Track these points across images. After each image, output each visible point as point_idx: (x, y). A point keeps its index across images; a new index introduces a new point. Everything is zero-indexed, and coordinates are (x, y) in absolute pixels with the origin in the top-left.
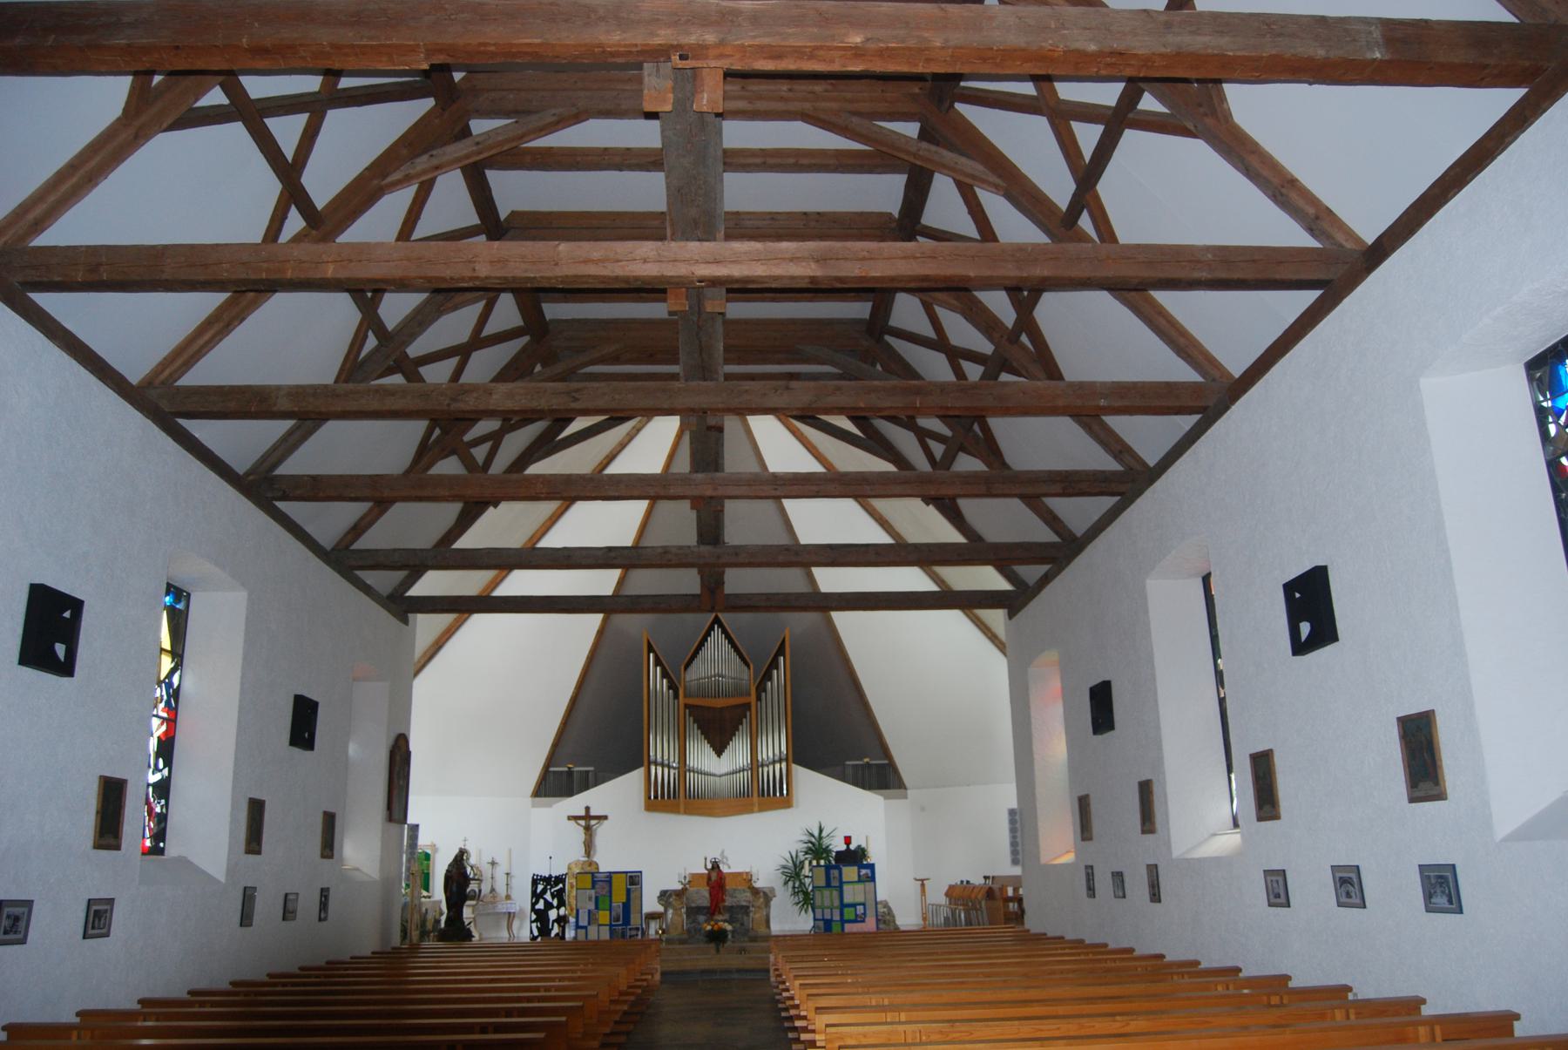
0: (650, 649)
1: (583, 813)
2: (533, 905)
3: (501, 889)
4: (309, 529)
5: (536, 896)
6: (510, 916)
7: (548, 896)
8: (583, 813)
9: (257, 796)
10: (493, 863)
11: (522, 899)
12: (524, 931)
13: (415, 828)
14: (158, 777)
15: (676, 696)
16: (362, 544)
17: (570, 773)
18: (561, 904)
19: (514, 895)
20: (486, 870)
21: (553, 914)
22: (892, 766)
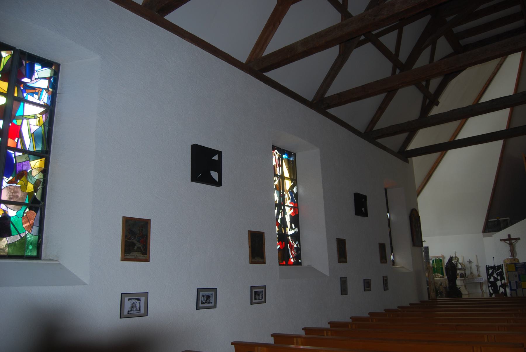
1: (507, 238)
2: (489, 279)
3: (475, 271)
4: (351, 124)
5: (489, 275)
6: (481, 284)
7: (495, 275)
8: (507, 238)
9: (382, 242)
10: (470, 262)
11: (484, 277)
12: (487, 290)
13: (427, 248)
14: (292, 232)
16: (377, 127)
17: (498, 221)
18: (502, 278)
19: (481, 275)
20: (467, 265)
21: (499, 283)
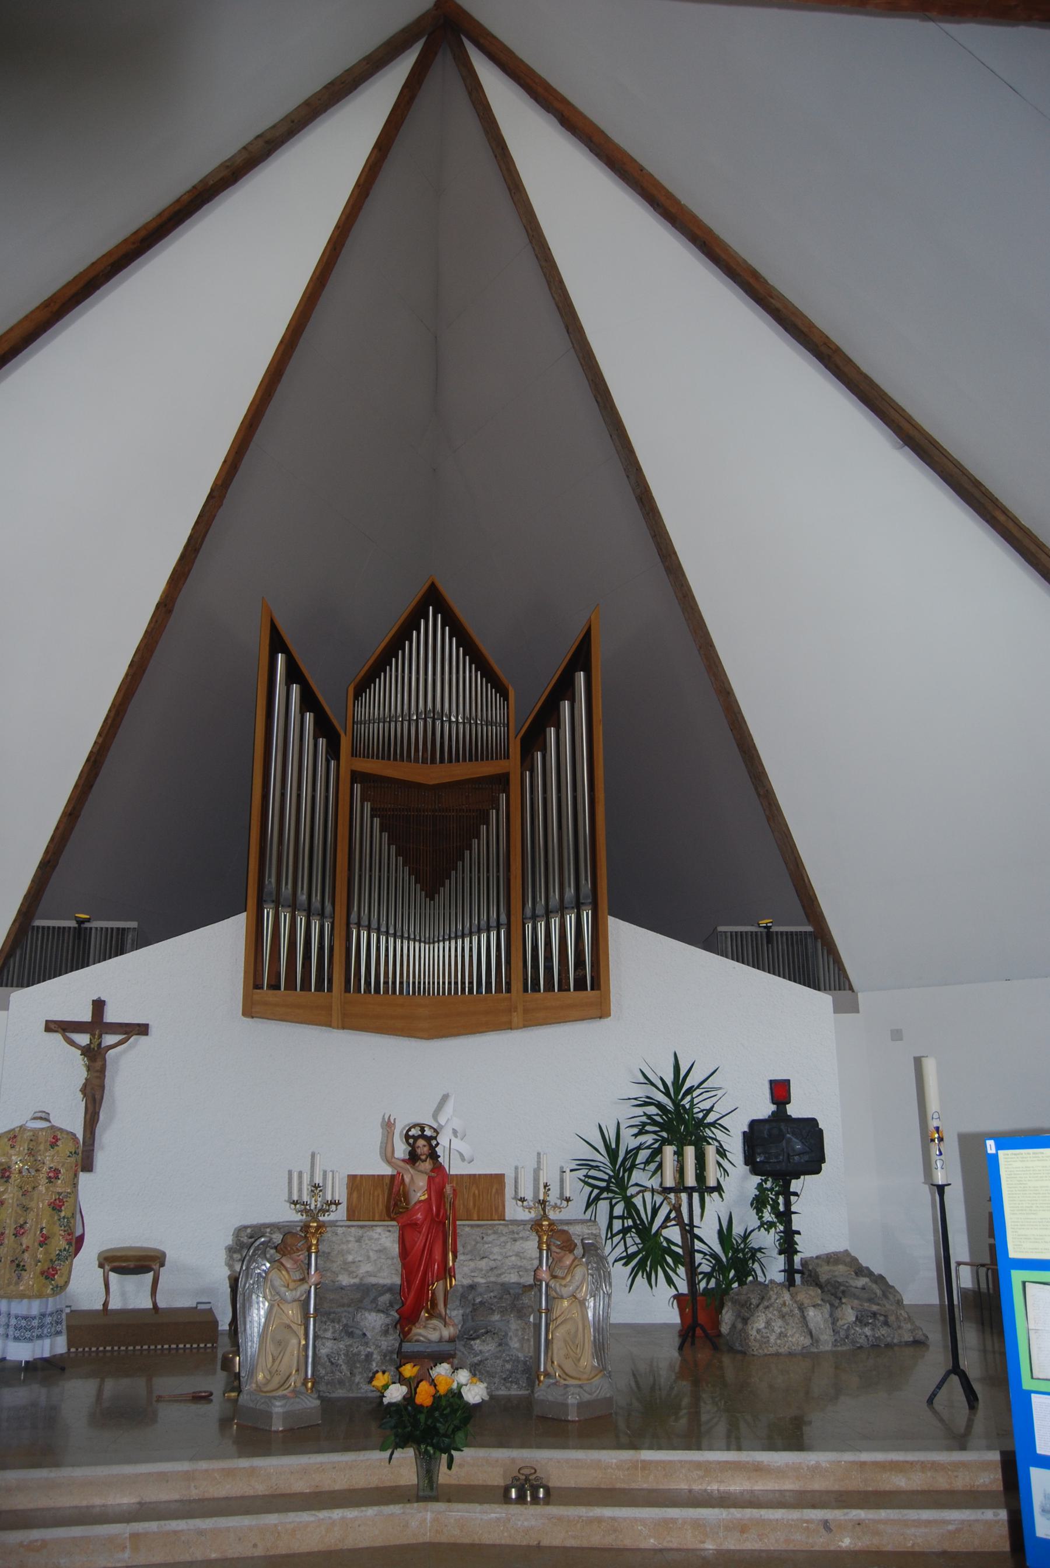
0: (277, 643)
1: (86, 1016)
8: (86, 1016)
15: (333, 751)
22: (822, 934)
